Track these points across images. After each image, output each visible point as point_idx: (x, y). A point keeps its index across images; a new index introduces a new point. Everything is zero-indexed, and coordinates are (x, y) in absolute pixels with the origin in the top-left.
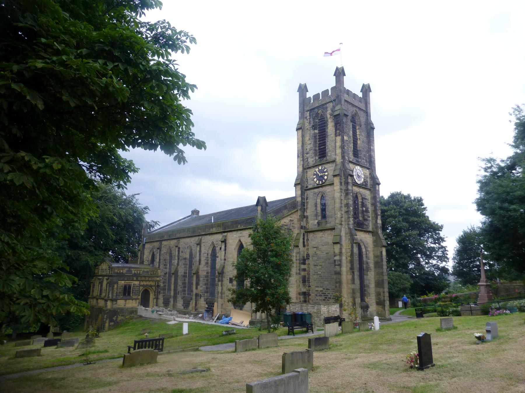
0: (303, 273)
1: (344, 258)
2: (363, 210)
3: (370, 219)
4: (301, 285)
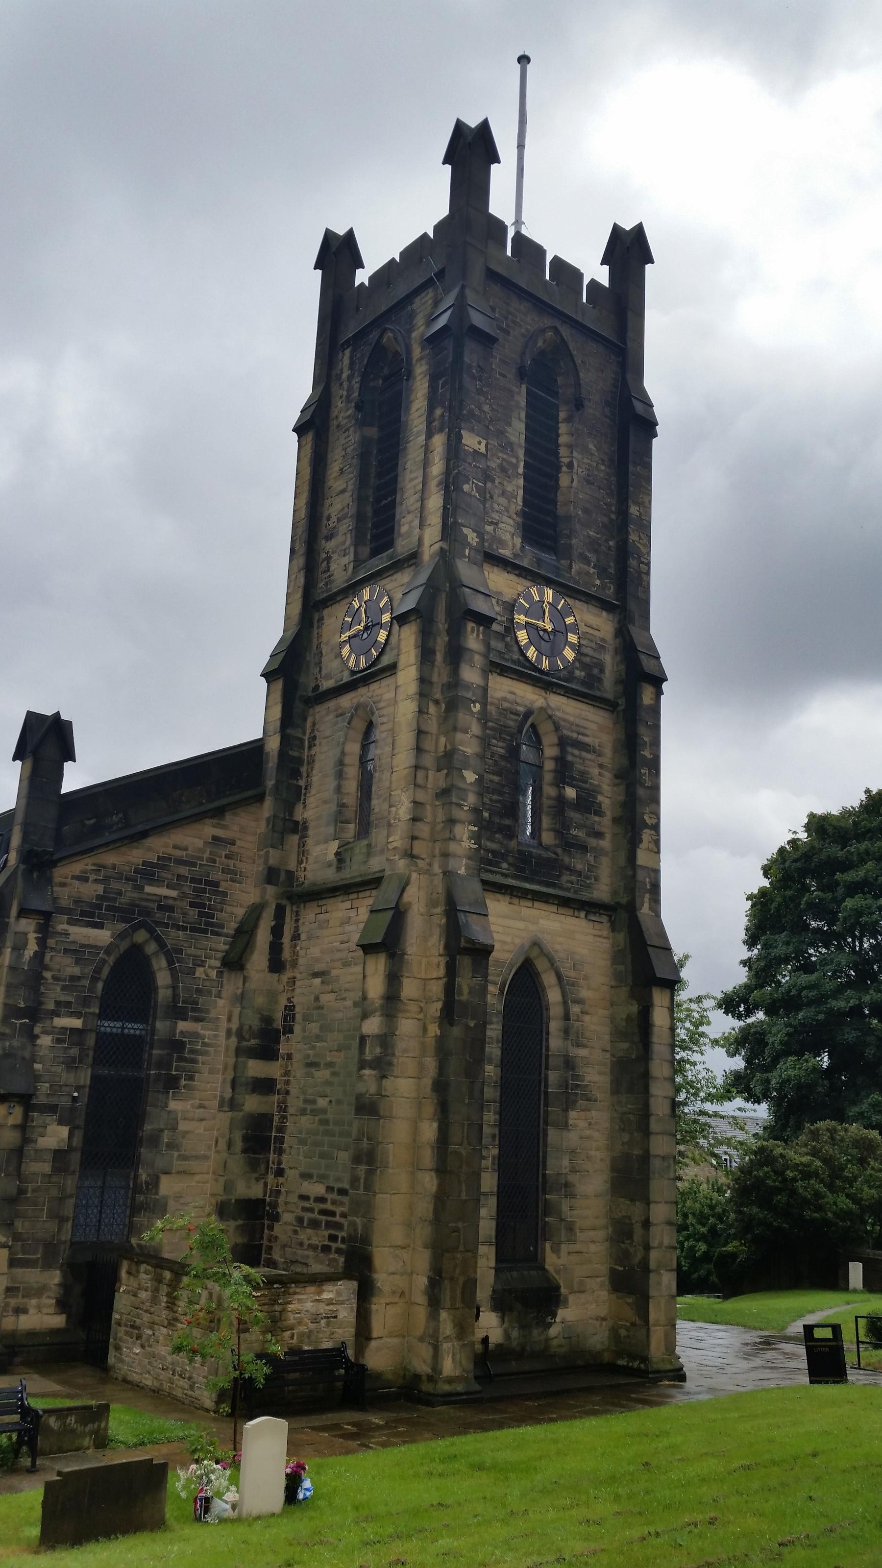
0: (252, 1103)
1: (407, 1026)
2: (561, 800)
3: (605, 844)
4: (237, 1163)
